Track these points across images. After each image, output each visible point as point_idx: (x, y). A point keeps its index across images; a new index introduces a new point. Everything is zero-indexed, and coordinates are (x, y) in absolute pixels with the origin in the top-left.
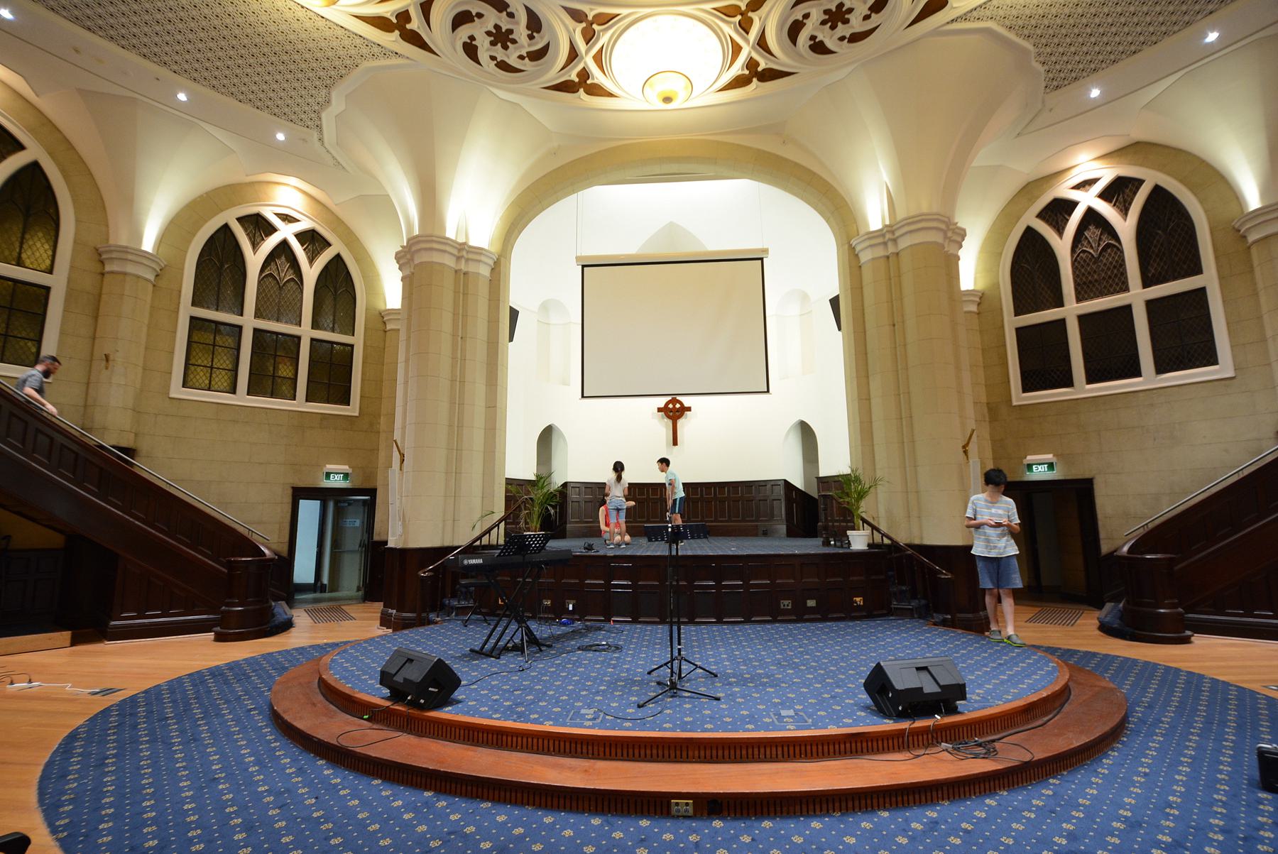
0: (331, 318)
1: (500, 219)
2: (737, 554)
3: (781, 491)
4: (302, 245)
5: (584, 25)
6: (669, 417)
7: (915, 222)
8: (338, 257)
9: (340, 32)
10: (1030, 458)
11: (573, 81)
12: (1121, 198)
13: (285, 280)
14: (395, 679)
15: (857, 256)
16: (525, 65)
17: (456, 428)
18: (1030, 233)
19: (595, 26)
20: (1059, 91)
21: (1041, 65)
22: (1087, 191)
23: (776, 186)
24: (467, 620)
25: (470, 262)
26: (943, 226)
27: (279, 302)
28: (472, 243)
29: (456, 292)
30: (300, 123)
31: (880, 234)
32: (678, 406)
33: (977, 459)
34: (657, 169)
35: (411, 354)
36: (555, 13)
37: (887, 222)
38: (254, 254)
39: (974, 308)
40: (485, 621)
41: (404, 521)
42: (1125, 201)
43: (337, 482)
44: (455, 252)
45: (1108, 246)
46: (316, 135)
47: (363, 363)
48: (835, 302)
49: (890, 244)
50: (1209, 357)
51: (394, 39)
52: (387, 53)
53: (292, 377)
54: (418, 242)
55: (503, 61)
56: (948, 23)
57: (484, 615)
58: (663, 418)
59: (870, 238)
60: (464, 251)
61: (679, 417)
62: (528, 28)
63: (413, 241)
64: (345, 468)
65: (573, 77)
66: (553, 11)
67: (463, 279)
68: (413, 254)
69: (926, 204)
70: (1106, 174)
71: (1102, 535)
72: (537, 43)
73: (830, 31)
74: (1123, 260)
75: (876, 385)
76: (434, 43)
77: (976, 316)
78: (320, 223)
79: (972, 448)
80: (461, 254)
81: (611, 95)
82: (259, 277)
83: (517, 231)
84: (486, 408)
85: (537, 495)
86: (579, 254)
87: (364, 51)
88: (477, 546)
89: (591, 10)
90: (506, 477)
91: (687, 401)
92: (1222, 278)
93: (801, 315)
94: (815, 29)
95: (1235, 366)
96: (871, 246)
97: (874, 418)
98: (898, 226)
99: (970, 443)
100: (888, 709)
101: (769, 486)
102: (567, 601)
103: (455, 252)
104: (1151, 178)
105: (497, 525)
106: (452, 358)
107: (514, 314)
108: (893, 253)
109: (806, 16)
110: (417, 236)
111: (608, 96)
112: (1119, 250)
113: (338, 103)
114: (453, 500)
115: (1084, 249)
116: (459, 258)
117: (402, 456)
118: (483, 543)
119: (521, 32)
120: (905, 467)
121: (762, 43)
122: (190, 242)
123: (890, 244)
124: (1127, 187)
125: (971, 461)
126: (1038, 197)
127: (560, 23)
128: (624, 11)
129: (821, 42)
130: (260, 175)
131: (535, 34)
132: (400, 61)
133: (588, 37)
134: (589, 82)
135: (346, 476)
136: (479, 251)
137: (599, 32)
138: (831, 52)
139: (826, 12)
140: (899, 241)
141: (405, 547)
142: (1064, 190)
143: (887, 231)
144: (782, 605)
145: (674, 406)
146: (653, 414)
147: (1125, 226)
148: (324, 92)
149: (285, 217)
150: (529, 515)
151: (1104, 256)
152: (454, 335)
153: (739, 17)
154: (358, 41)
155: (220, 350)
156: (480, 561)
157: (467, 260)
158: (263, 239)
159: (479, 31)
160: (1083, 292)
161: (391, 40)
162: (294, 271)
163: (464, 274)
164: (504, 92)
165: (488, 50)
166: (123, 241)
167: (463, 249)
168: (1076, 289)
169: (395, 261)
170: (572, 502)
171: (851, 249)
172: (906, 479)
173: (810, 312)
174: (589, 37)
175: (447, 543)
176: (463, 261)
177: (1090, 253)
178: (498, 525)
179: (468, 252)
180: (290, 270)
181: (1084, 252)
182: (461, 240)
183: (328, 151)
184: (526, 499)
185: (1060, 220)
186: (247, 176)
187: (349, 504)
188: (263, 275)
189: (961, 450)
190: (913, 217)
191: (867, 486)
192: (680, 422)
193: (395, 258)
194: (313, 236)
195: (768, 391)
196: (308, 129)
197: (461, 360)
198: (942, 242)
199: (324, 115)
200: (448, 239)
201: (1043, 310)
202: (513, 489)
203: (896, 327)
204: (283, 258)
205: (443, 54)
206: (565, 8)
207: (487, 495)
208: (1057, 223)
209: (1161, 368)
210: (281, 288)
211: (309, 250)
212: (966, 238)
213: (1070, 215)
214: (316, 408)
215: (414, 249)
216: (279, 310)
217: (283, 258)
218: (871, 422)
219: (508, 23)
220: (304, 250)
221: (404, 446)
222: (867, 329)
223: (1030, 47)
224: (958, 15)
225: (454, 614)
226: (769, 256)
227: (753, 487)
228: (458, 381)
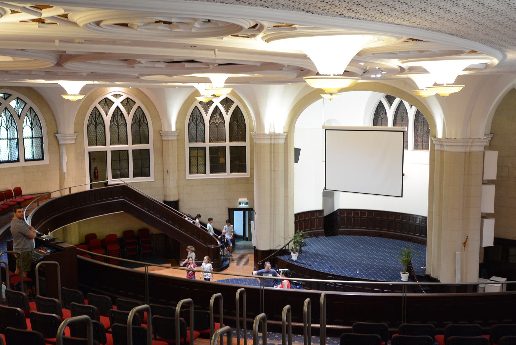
1: (288, 116)
14: (107, 334)
28: (277, 133)
31: (440, 139)
47: (250, 153)
60: (273, 136)
64: (246, 200)
67: (273, 147)
82: (209, 125)
107: (297, 151)
116: (271, 139)
122: (185, 118)
136: (279, 135)
152: (271, 170)
155: (208, 270)
158: (209, 107)
162: (221, 118)
166: (166, 130)
188: (211, 123)
194: (227, 100)
195: (402, 197)
211: (226, 107)
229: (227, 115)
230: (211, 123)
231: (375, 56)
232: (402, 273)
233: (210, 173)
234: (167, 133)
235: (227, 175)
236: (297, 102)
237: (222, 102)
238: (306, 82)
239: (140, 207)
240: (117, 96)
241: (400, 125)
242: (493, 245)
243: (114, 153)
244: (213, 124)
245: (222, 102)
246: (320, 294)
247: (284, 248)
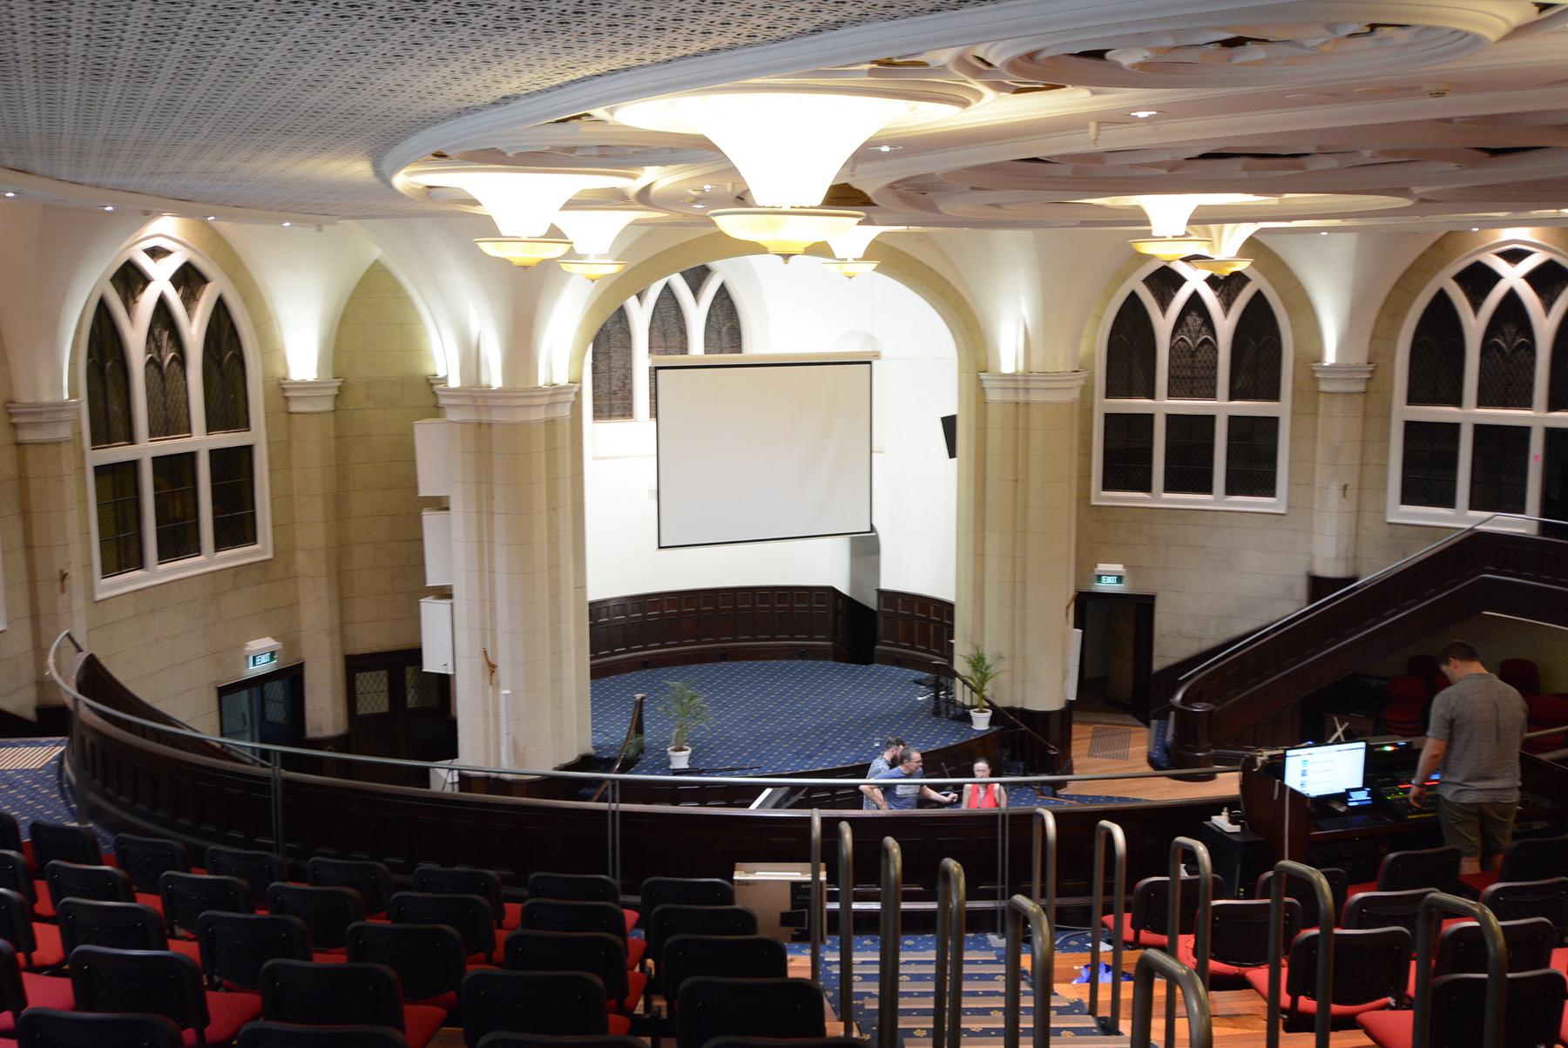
12: (1225, 291)
18: (1133, 298)
23: (905, 284)
31: (1012, 378)
42: (1229, 295)
43: (263, 666)
48: (949, 424)
49: (1021, 393)
50: (1268, 488)
60: (555, 390)
71: (1156, 653)
74: (1216, 363)
75: (992, 543)
92: (1293, 413)
95: (1288, 503)
100: (346, 769)
104: (1258, 282)
112: (1215, 349)
115: (1184, 337)
123: (1021, 393)
147: (1225, 325)
160: (1175, 387)
177: (1187, 342)
181: (1182, 340)
195: (660, 548)
208: (1163, 295)
209: (1231, 490)
228: (554, 566)
231: (549, 143)
232: (672, 750)
233: (1103, 490)
234: (37, 410)
235: (209, 561)
238: (713, 224)
239: (1529, 580)
240: (1514, 256)
241: (661, 351)
242: (425, 669)
243: (1483, 432)
246: (808, 820)
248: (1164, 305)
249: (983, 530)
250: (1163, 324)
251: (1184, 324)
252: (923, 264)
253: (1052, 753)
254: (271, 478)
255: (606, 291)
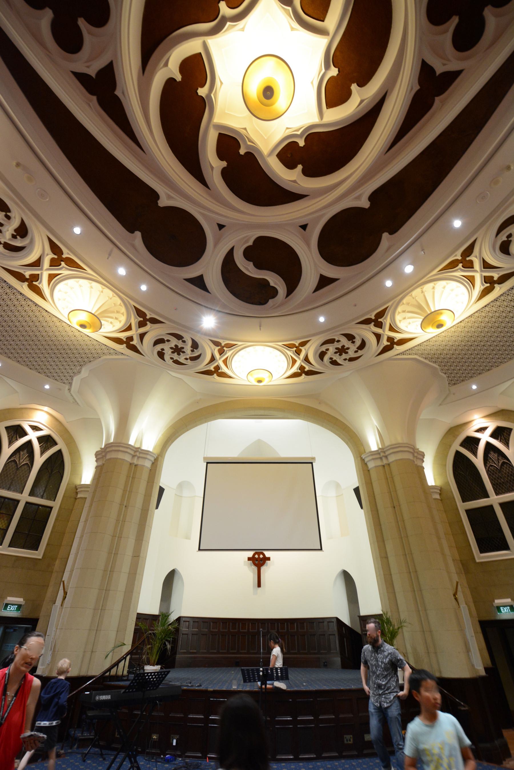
0: (44, 489)
1: (162, 435)
2: (308, 689)
3: (334, 627)
4: (40, 444)
5: (219, 347)
6: (255, 565)
7: (396, 448)
8: (60, 452)
9: (95, 343)
10: (497, 602)
11: (211, 370)
12: (502, 437)
13: (22, 464)
15: (366, 464)
16: (187, 362)
17: (109, 572)
18: (458, 454)
19: (225, 348)
20: (456, 386)
21: (444, 374)
22: (483, 433)
24: (86, 754)
25: (140, 459)
26: (411, 450)
27: (14, 477)
28: (144, 448)
29: (128, 477)
30: (60, 381)
31: (377, 453)
32: (261, 556)
33: (465, 605)
34: (252, 413)
35: (90, 516)
36: (206, 343)
37: (380, 447)
38: (9, 448)
39: (438, 497)
40: (102, 755)
41: (54, 651)
42: (505, 439)
43: (12, 612)
44: (132, 453)
45: (504, 463)
46: (67, 387)
48: (357, 491)
49: (384, 459)
51: (122, 348)
52: (116, 353)
53: (5, 528)
54: (112, 446)
55: (177, 360)
56: (396, 355)
57: (101, 748)
58: (251, 566)
59: (372, 455)
61: (263, 564)
62: (192, 347)
63: (108, 446)
64: (20, 600)
65: (212, 368)
66: (206, 343)
67: (134, 467)
68: (106, 453)
69: (399, 438)
70: (492, 426)
72: (195, 353)
73: (339, 356)
75: (390, 547)
76: (144, 352)
77: (440, 501)
78: (54, 431)
79: (460, 595)
80: (136, 454)
81: (230, 377)
83: (170, 441)
84: (132, 557)
85: (159, 629)
86: (205, 456)
87: (106, 351)
88: (107, 677)
89: (224, 342)
90: (138, 612)
91: (267, 554)
93: (337, 496)
94: (332, 355)
96: (373, 459)
97: (393, 572)
98: (388, 448)
99: (458, 592)
101: (326, 623)
102: (172, 735)
103: (132, 453)
105: (124, 658)
106: (117, 520)
107: (161, 491)
108: (386, 464)
109: (327, 350)
110: (112, 443)
111: (229, 378)
113: (85, 372)
114: (95, 632)
116: (134, 456)
117: (65, 593)
118: (111, 674)
119: (188, 348)
120: (419, 611)
121: (306, 359)
123: (384, 459)
124: (504, 432)
125: (461, 606)
126: (458, 436)
127: (207, 345)
128: (240, 343)
129: (335, 361)
130: (30, 405)
131: (195, 350)
132: (123, 357)
133: (221, 352)
134: (219, 371)
135: (19, 607)
136: (147, 452)
137: (227, 351)
138: (339, 365)
139: (336, 349)
140: (389, 457)
141: (50, 675)
142: (471, 432)
143: (382, 452)
144: (345, 740)
145: (259, 556)
146: (245, 562)
148: (78, 368)
149: (35, 427)
150: (151, 649)
151: (503, 469)
152: (121, 504)
153: (295, 349)
154: (104, 347)
156: (108, 697)
157: (139, 457)
159: (167, 348)
161: (122, 348)
163: (135, 466)
164: (176, 373)
165: (170, 355)
167: (137, 451)
168: (494, 488)
169: (95, 456)
170: (183, 634)
171: (363, 460)
172: (421, 621)
173: (342, 494)
174: (221, 352)
175: (83, 673)
176: (136, 458)
178: (125, 658)
179: (140, 453)
180: (27, 458)
182: (137, 446)
183: (71, 395)
184: (150, 634)
185: (473, 448)
186: (20, 405)
187: (15, 630)
188: (10, 460)
189: (453, 598)
190: (393, 445)
191: (396, 627)
192: (263, 569)
193: (95, 455)
195: (321, 549)
196: (64, 384)
197: (122, 521)
198: (412, 459)
199: (75, 379)
200: (130, 445)
201: (478, 499)
202: (143, 626)
203: (396, 508)
204: (25, 451)
205: (146, 355)
206: (211, 340)
207: (121, 629)
208: (472, 449)
210: (17, 469)
211: (43, 447)
212: (425, 457)
213: (478, 445)
214: (15, 552)
215: (108, 450)
216: (12, 483)
217: (25, 451)
218: (391, 575)
219: (182, 344)
220: (40, 446)
221: (68, 586)
222: (378, 509)
223: (437, 367)
224: (400, 352)
225: (76, 746)
226: (316, 461)
227: (315, 623)
229: (41, 457)
230: (10, 460)
236: (180, 417)
237: (40, 439)
244: (13, 463)
245: (40, 439)
247: (108, 674)
248: (475, 453)
249: (384, 541)
250: (478, 461)
251: (489, 459)
252: (323, 412)
253: (463, 708)
254: (55, 522)
255: (178, 420)
